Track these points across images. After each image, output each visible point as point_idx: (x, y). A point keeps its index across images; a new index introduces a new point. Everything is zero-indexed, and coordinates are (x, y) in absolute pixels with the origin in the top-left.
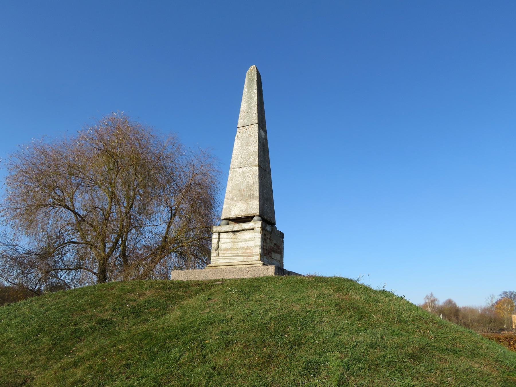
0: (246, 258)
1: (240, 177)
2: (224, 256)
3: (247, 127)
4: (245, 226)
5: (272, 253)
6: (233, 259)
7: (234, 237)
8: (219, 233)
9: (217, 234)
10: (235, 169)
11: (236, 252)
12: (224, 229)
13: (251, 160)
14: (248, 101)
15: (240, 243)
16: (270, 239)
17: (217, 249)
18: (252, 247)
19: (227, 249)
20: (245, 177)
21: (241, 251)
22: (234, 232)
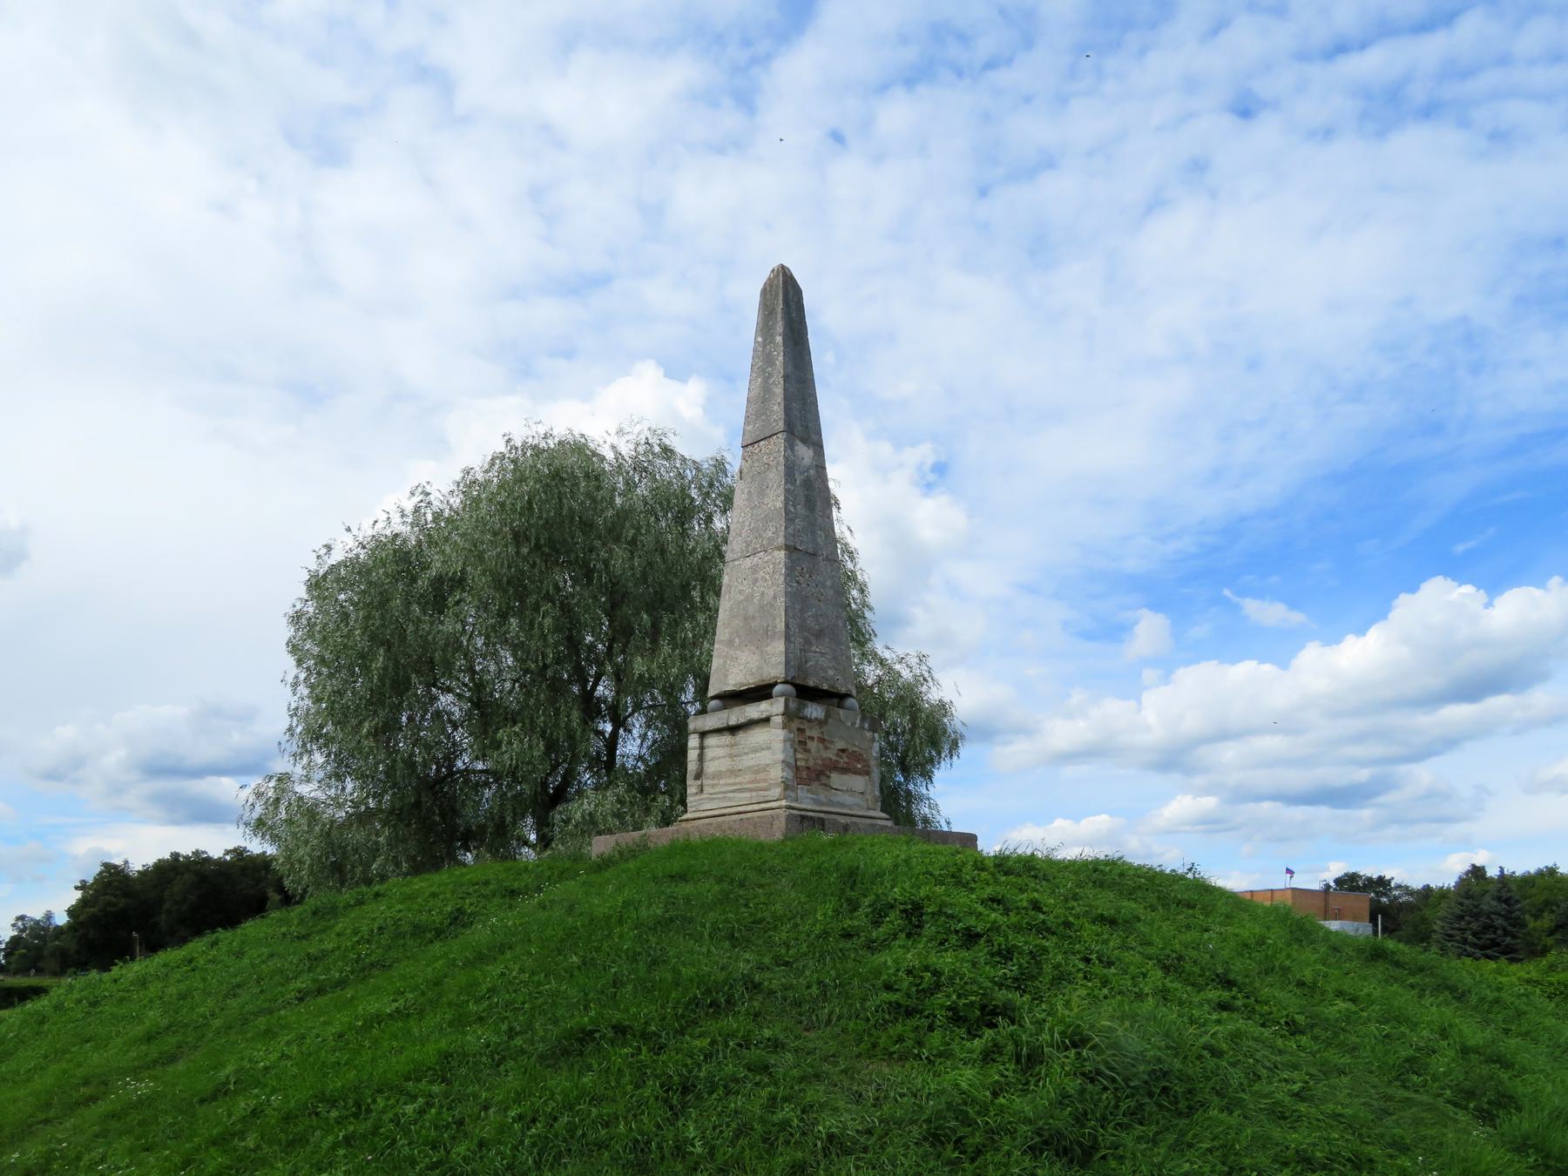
0: (754, 794)
1: (745, 582)
2: (712, 791)
3: (762, 443)
4: (754, 711)
5: (832, 775)
6: (730, 799)
7: (733, 742)
8: (703, 735)
9: (697, 736)
10: (736, 563)
11: (737, 780)
12: (710, 724)
13: (770, 534)
14: (764, 371)
15: (745, 757)
16: (822, 740)
17: (698, 776)
18: (768, 765)
19: (718, 775)
20: (756, 580)
21: (748, 777)
22: (733, 730)
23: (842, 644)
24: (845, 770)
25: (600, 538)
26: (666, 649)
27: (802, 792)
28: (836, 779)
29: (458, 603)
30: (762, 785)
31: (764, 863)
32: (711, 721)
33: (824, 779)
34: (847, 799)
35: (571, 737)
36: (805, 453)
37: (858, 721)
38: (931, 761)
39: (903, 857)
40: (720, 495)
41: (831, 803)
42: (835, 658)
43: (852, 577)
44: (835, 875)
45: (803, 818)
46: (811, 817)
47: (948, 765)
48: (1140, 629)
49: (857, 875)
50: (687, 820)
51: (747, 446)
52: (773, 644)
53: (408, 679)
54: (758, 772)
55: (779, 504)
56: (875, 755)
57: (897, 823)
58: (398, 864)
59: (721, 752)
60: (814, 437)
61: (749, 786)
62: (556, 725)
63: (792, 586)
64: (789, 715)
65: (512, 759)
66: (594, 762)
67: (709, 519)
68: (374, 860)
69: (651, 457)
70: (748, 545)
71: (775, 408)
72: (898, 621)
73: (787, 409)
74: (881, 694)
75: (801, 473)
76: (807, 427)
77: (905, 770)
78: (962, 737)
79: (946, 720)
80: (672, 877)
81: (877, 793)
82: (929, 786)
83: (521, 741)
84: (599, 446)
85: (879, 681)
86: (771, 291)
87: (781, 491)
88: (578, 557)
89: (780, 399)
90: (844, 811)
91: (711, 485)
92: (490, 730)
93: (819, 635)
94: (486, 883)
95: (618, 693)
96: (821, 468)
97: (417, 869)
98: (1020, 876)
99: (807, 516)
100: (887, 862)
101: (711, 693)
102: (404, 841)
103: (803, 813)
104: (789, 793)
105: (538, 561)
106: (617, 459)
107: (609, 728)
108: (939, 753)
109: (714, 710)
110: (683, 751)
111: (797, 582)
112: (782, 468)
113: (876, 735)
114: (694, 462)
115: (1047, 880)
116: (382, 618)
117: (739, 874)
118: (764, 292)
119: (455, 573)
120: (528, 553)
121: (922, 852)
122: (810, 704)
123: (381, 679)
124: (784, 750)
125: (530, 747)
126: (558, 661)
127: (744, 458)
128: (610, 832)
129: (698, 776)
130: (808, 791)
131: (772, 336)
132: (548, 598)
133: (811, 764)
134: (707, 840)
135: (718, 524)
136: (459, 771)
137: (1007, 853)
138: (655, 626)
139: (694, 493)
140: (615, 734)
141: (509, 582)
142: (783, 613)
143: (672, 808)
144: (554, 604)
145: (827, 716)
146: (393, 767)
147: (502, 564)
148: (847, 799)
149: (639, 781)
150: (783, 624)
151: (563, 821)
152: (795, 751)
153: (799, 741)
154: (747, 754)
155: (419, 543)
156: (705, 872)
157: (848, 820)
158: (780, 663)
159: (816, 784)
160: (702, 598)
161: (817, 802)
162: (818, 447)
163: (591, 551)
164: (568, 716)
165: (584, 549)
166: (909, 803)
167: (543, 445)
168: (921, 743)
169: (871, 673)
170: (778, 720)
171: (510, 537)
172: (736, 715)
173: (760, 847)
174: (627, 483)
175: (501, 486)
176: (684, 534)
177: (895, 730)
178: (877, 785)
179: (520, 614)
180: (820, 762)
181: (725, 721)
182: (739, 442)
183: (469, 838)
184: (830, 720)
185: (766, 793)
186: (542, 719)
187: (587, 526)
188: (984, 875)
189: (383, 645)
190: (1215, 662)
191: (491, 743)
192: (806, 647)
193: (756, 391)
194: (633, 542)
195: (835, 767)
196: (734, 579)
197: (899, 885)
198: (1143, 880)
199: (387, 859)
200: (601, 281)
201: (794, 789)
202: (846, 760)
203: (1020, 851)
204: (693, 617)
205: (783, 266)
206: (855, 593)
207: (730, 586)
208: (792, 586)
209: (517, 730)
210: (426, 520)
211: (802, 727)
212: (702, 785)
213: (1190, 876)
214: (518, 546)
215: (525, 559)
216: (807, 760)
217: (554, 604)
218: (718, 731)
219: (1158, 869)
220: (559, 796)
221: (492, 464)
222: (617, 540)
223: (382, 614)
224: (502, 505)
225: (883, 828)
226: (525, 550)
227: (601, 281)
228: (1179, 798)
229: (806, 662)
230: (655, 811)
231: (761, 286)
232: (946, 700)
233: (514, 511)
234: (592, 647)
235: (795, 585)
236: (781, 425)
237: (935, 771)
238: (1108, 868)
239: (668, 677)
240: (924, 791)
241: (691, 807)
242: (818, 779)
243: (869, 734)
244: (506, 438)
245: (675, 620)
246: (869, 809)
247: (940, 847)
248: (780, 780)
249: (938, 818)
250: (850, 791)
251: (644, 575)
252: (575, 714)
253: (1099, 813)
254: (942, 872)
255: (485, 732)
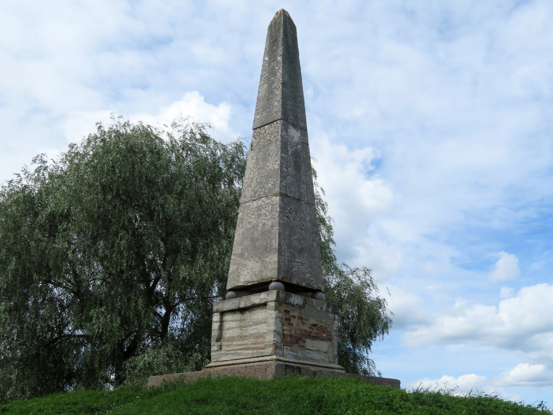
0: (255, 351)
1: (253, 217)
2: (227, 349)
3: (266, 127)
4: (256, 299)
6: (239, 354)
7: (242, 318)
8: (222, 313)
10: (247, 204)
11: (244, 342)
12: (227, 307)
13: (270, 186)
14: (269, 79)
15: (250, 328)
16: (301, 318)
18: (265, 333)
19: (232, 339)
20: (260, 215)
21: (251, 341)
22: (242, 310)
23: (315, 258)
24: (315, 338)
25: (159, 191)
26: (201, 262)
27: (287, 351)
28: (309, 343)
29: (65, 230)
30: (260, 346)
31: (260, 393)
32: (229, 305)
33: (301, 343)
34: (316, 356)
35: (138, 315)
36: (295, 134)
37: (325, 307)
38: (371, 336)
39: (354, 391)
40: (238, 166)
41: (305, 358)
42: (311, 267)
43: (322, 221)
44: (307, 401)
45: (287, 366)
46: (292, 366)
47: (381, 339)
48: (500, 264)
49: (322, 401)
50: (211, 367)
51: (256, 129)
52: (270, 257)
53: (31, 276)
54: (258, 337)
55: (277, 167)
56: (335, 328)
57: (347, 371)
58: (23, 392)
59: (234, 324)
60: (302, 124)
61: (252, 346)
62: (129, 308)
63: (283, 220)
64: (279, 302)
65: (99, 328)
66: (153, 333)
67: (231, 182)
68: (8, 389)
69: (194, 141)
70: (255, 193)
71: (276, 104)
72: (352, 255)
73: (284, 105)
74: (339, 293)
75: (292, 147)
76: (297, 117)
77: (353, 341)
78: (391, 321)
79: (381, 310)
80: (198, 401)
81: (336, 353)
82: (368, 351)
83: (106, 317)
84: (159, 132)
85: (339, 285)
86: (275, 27)
87: (278, 158)
88: (144, 202)
89: (279, 98)
90: (314, 363)
91: (233, 160)
92: (85, 310)
93: (301, 251)
94: (76, 404)
95: (169, 289)
96: (305, 144)
97: (36, 393)
98: (431, 406)
99: (295, 175)
100: (343, 394)
101: (229, 287)
102: (28, 378)
103: (287, 364)
104: (277, 351)
105: (118, 204)
106: (171, 142)
107: (164, 311)
108: (375, 331)
109: (230, 298)
110: (209, 324)
111: (287, 217)
112: (279, 143)
113: (336, 316)
114: (222, 145)
115: (448, 409)
116: (15, 238)
117: (243, 400)
118: (271, 27)
119: (63, 211)
120: (112, 199)
121: (366, 389)
122: (293, 295)
123: (14, 276)
124: (276, 324)
125: (111, 321)
126: (130, 268)
127: (254, 137)
128: (161, 374)
129: (219, 339)
130: (290, 350)
131: (275, 57)
132: (124, 227)
133: (293, 333)
134: (222, 379)
135: (237, 185)
136: (65, 336)
137: (422, 391)
138: (194, 246)
139: (222, 165)
140: (167, 315)
141: (99, 217)
142: (277, 237)
143: (202, 360)
144: (127, 231)
145: (305, 303)
146: (21, 331)
147: (95, 205)
148: (316, 356)
149: (182, 344)
150: (277, 244)
151: (132, 367)
152: (283, 324)
153: (286, 318)
154: (251, 326)
155: (40, 192)
156: (220, 398)
157: (316, 369)
158: (274, 269)
159: (296, 345)
160: (226, 230)
161: (296, 357)
162: (304, 130)
163: (153, 199)
164: (136, 302)
165: (148, 198)
166: (355, 361)
167: (122, 131)
168: (364, 325)
169: (333, 281)
170: (272, 304)
171: (100, 188)
172: (244, 302)
173: (258, 383)
174: (177, 157)
175: (94, 155)
176: (215, 189)
177: (348, 317)
178: (336, 347)
179: (106, 239)
180: (299, 332)
181: (237, 305)
182: (251, 126)
183: (70, 377)
184: (306, 306)
185: (263, 351)
186: (119, 303)
187: (150, 183)
188: (408, 404)
189: (15, 254)
190: (545, 285)
191: (86, 318)
192: (292, 259)
193: (263, 93)
194: (181, 194)
195: (309, 336)
196: (245, 215)
197: (351, 409)
198: (510, 411)
199: (17, 389)
200: (166, 41)
201: (281, 349)
202: (316, 331)
203: (430, 390)
204: (219, 243)
205: (284, 11)
206: (324, 231)
207: (242, 219)
208: (283, 220)
209: (103, 310)
210: (45, 178)
211: (288, 309)
212: (221, 345)
213: (540, 409)
214: (105, 193)
215: (110, 202)
216: (290, 331)
217: (127, 231)
218: (233, 311)
219: (519, 404)
220: (132, 351)
221: (89, 142)
222: (170, 192)
223: (15, 235)
224: (95, 167)
225: (339, 374)
226: (109, 197)
227: (166, 41)
228: (520, 365)
229: (292, 268)
230: (191, 363)
231: (268, 23)
232: (381, 298)
233: (102, 171)
234: (152, 261)
235: (286, 219)
236: (279, 115)
237: (373, 342)
238: (487, 403)
239: (201, 279)
240: (365, 354)
241: (214, 359)
242: (297, 342)
243: (331, 316)
244: (98, 125)
245: (207, 244)
246: (330, 362)
247: (378, 386)
248: (272, 343)
249: (373, 371)
250: (318, 351)
251: (188, 214)
252: (140, 301)
253: (470, 373)
254: (380, 402)
255: (82, 311)
